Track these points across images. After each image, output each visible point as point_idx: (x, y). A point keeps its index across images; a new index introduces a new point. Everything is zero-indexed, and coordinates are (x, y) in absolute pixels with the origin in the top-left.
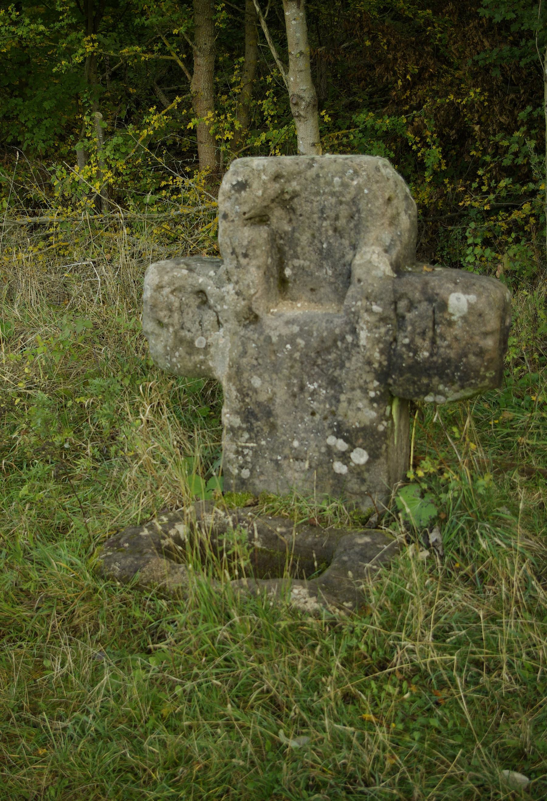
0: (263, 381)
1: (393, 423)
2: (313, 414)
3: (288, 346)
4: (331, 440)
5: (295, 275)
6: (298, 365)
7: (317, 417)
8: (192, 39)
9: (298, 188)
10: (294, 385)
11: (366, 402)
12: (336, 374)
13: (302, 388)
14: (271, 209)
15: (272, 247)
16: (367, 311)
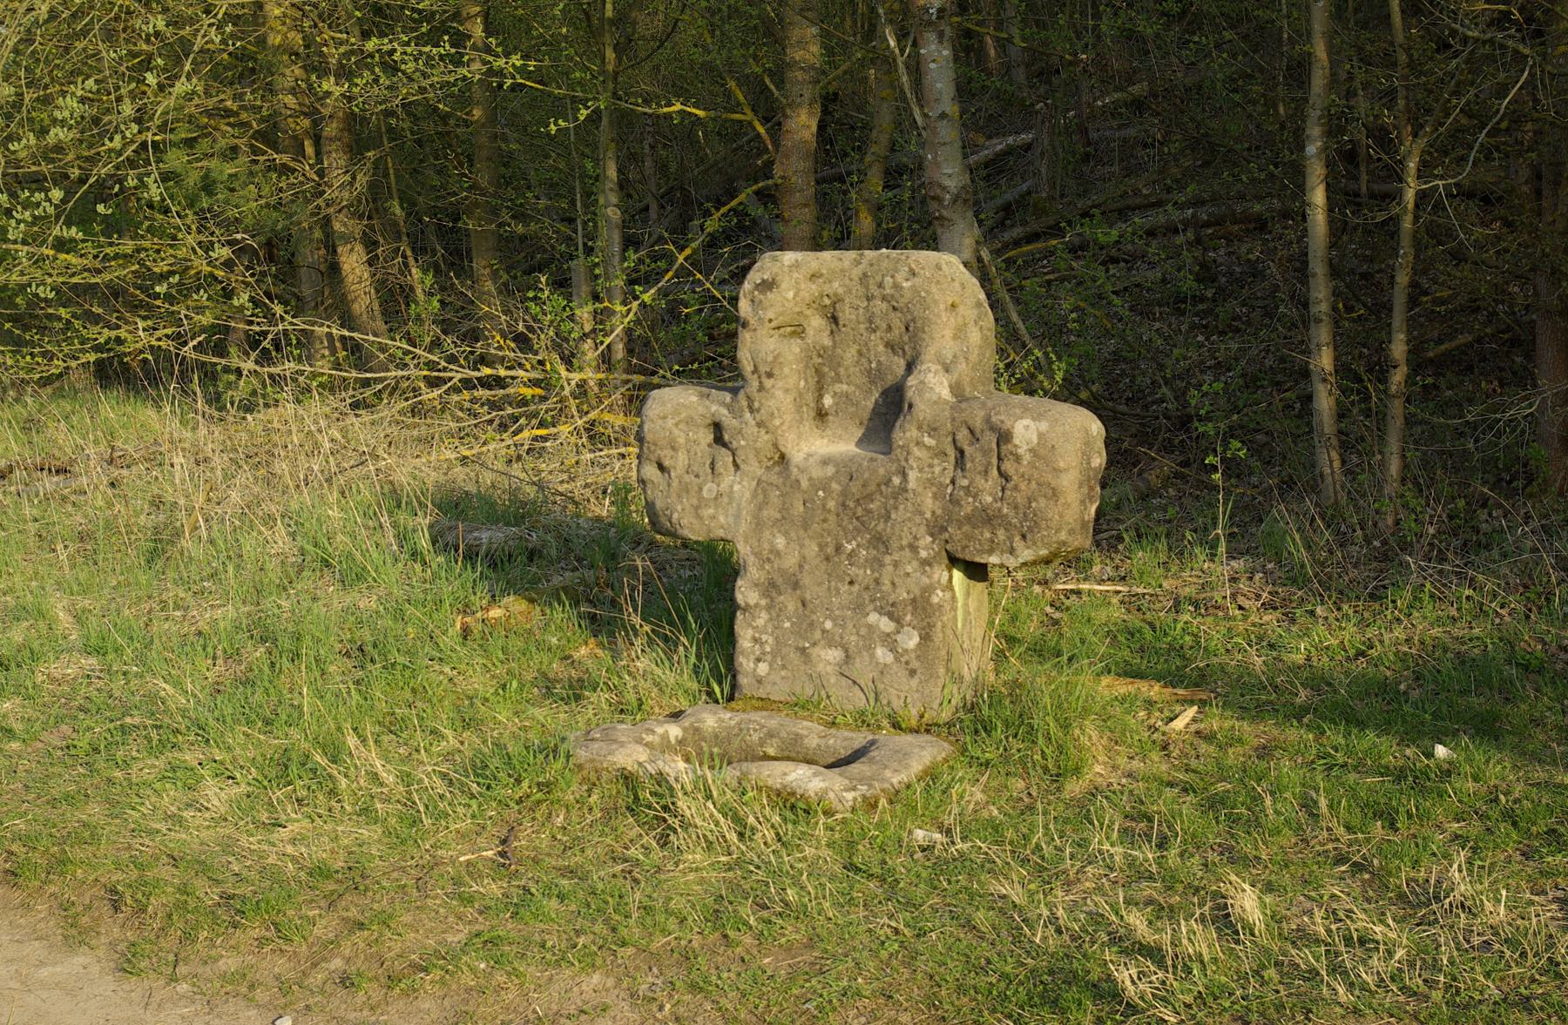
0: (789, 540)
1: (954, 598)
2: (851, 583)
3: (821, 493)
4: (873, 618)
5: (837, 404)
6: (832, 518)
7: (856, 588)
8: (780, 84)
9: (840, 291)
10: (827, 545)
11: (915, 563)
12: (879, 528)
13: (838, 549)
14: (807, 317)
15: (807, 367)
16: (918, 444)
